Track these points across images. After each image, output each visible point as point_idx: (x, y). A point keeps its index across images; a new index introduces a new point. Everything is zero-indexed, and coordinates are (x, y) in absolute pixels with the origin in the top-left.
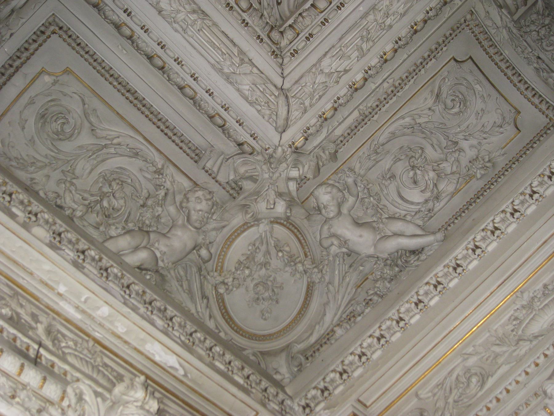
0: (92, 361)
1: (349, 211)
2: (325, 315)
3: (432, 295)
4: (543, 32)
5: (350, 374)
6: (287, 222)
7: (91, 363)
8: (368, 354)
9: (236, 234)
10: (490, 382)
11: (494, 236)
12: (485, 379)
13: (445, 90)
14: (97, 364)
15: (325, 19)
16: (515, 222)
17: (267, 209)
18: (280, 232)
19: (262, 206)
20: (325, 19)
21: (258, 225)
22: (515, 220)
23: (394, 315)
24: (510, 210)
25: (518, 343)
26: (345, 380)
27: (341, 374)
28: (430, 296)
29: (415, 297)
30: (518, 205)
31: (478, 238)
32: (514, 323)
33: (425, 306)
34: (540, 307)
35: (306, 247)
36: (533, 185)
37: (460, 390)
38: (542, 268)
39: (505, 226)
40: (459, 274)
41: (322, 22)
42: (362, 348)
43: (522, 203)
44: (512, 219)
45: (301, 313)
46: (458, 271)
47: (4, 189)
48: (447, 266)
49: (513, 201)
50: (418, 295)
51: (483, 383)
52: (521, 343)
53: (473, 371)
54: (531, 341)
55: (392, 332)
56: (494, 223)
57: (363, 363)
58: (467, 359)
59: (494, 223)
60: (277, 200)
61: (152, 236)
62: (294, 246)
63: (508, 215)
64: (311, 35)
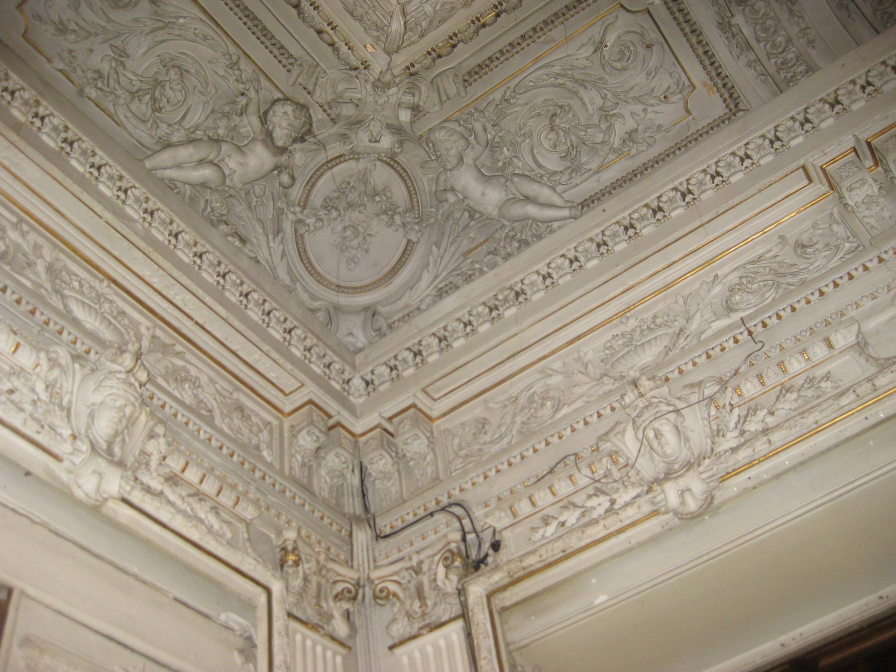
0: (97, 307)
1: (475, 161)
2: (419, 279)
3: (888, 78)
6: (391, 160)
7: (96, 310)
9: (338, 161)
10: (565, 411)
11: (864, 92)
12: (561, 406)
13: (610, 39)
14: (103, 310)
17: (370, 141)
18: (382, 175)
19: (362, 138)
21: (358, 159)
23: (681, 184)
24: (861, 82)
25: (601, 378)
26: (602, 254)
27: (599, 246)
28: (885, 79)
29: (714, 167)
30: (874, 77)
32: (607, 352)
35: (414, 196)
37: (532, 411)
40: (807, 131)
42: (523, 284)
44: (861, 95)
45: (395, 270)
46: (775, 146)
47: (5, 84)
48: (763, 137)
50: (604, 235)
51: (557, 409)
52: (605, 378)
53: (552, 393)
54: (616, 380)
55: (535, 289)
56: (688, 184)
58: (551, 376)
59: (688, 184)
60: (383, 132)
61: (225, 147)
62: (399, 193)
63: (858, 87)
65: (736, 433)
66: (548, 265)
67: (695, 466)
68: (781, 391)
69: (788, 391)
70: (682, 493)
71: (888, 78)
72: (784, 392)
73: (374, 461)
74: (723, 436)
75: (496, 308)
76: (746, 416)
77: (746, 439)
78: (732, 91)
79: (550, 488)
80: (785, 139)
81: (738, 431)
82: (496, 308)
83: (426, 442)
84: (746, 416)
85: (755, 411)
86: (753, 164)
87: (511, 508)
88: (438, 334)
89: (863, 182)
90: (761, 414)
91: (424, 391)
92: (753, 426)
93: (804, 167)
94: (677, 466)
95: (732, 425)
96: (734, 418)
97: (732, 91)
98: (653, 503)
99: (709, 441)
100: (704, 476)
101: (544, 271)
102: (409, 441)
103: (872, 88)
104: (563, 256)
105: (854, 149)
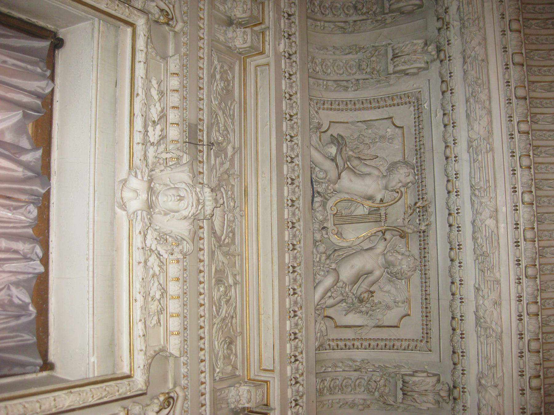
4: (373, 384)
5: (288, 163)
8: (290, 187)
15: (516, 191)
16: (290, 308)
20: (516, 191)
22: (291, 332)
24: (299, 357)
30: (297, 298)
31: (300, 367)
33: (290, 294)
34: (226, 216)
36: (301, 408)
38: (248, 272)
39: (294, 390)
41: (516, 188)
43: (297, 369)
49: (296, 63)
57: (288, 200)
64: (517, 228)
65: (153, 248)
66: (298, 208)
67: (148, 211)
68: (163, 289)
69: (162, 294)
70: (135, 191)
71: (293, 350)
72: (162, 291)
73: (245, 37)
74: (156, 239)
75: (289, 78)
76: (160, 259)
77: (148, 251)
78: (331, 347)
79: (177, 91)
80: (292, 320)
81: (154, 249)
82: (292, 184)
83: (238, 46)
84: (160, 259)
85: (160, 266)
86: (289, 249)
87: (177, 74)
88: (294, 56)
89: (249, 402)
90: (157, 269)
91: (268, 64)
92: (153, 260)
93: (273, 371)
94: (154, 198)
95: (159, 249)
96: (162, 252)
97: (331, 347)
98: (139, 263)
99: (157, 228)
100: (139, 212)
101: (296, 182)
102: (245, 7)
103: (292, 316)
104: (297, 114)
105: (267, 405)
